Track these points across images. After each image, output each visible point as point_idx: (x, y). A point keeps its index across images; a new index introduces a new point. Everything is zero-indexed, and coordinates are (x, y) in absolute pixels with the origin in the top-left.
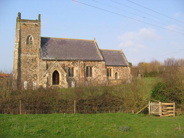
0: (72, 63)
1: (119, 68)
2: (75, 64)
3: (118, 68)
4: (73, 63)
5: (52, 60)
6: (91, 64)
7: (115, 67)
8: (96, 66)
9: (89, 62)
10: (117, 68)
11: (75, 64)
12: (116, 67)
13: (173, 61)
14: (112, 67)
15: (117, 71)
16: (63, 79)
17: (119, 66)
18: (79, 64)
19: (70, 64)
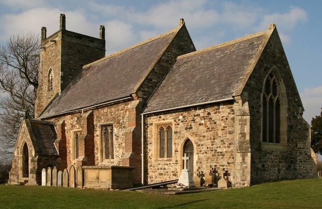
1: (198, 119)
3: (194, 120)
6: (109, 116)
15: (187, 135)
16: (176, 151)
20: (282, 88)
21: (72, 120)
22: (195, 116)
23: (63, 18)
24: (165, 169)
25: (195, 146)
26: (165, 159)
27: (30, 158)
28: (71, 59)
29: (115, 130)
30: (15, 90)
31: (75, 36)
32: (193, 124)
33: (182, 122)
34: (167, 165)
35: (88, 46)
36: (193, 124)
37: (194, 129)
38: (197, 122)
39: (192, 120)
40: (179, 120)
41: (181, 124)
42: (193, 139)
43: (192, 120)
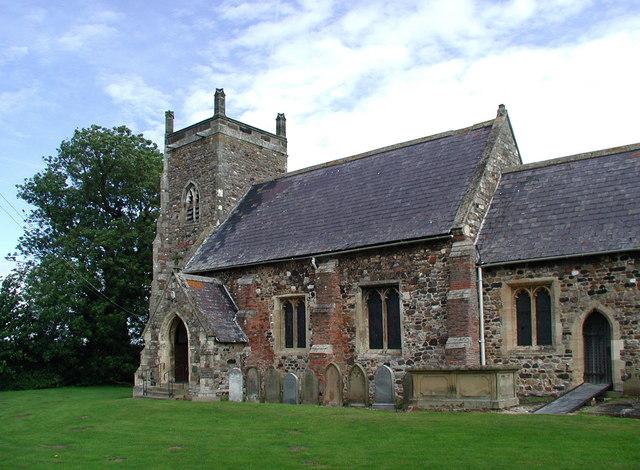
0: (289, 274)
1: (620, 277)
2: (306, 280)
3: (610, 279)
4: (294, 273)
5: (92, 460)
6: (386, 269)
7: (575, 273)
8: (415, 281)
9: (375, 259)
10: (598, 274)
11: (306, 280)
12: (589, 267)
13: (128, 151)
14: (546, 276)
15: (594, 303)
16: (566, 333)
17: (613, 256)
18: (478, 288)
19: (284, 282)
20: (394, 154)
21: (276, 277)
22: (611, 270)
23: (219, 96)
24: (535, 366)
25: (615, 325)
26: (534, 347)
27: (308, 314)
28: (234, 168)
29: (405, 296)
30: (42, 231)
31: (241, 129)
32: (607, 284)
33: (579, 280)
34: (542, 358)
35: (261, 147)
36: (607, 284)
37: (612, 292)
38: (618, 282)
39: (605, 278)
40: (571, 277)
41: (577, 285)
42: (609, 312)
43: (605, 278)
